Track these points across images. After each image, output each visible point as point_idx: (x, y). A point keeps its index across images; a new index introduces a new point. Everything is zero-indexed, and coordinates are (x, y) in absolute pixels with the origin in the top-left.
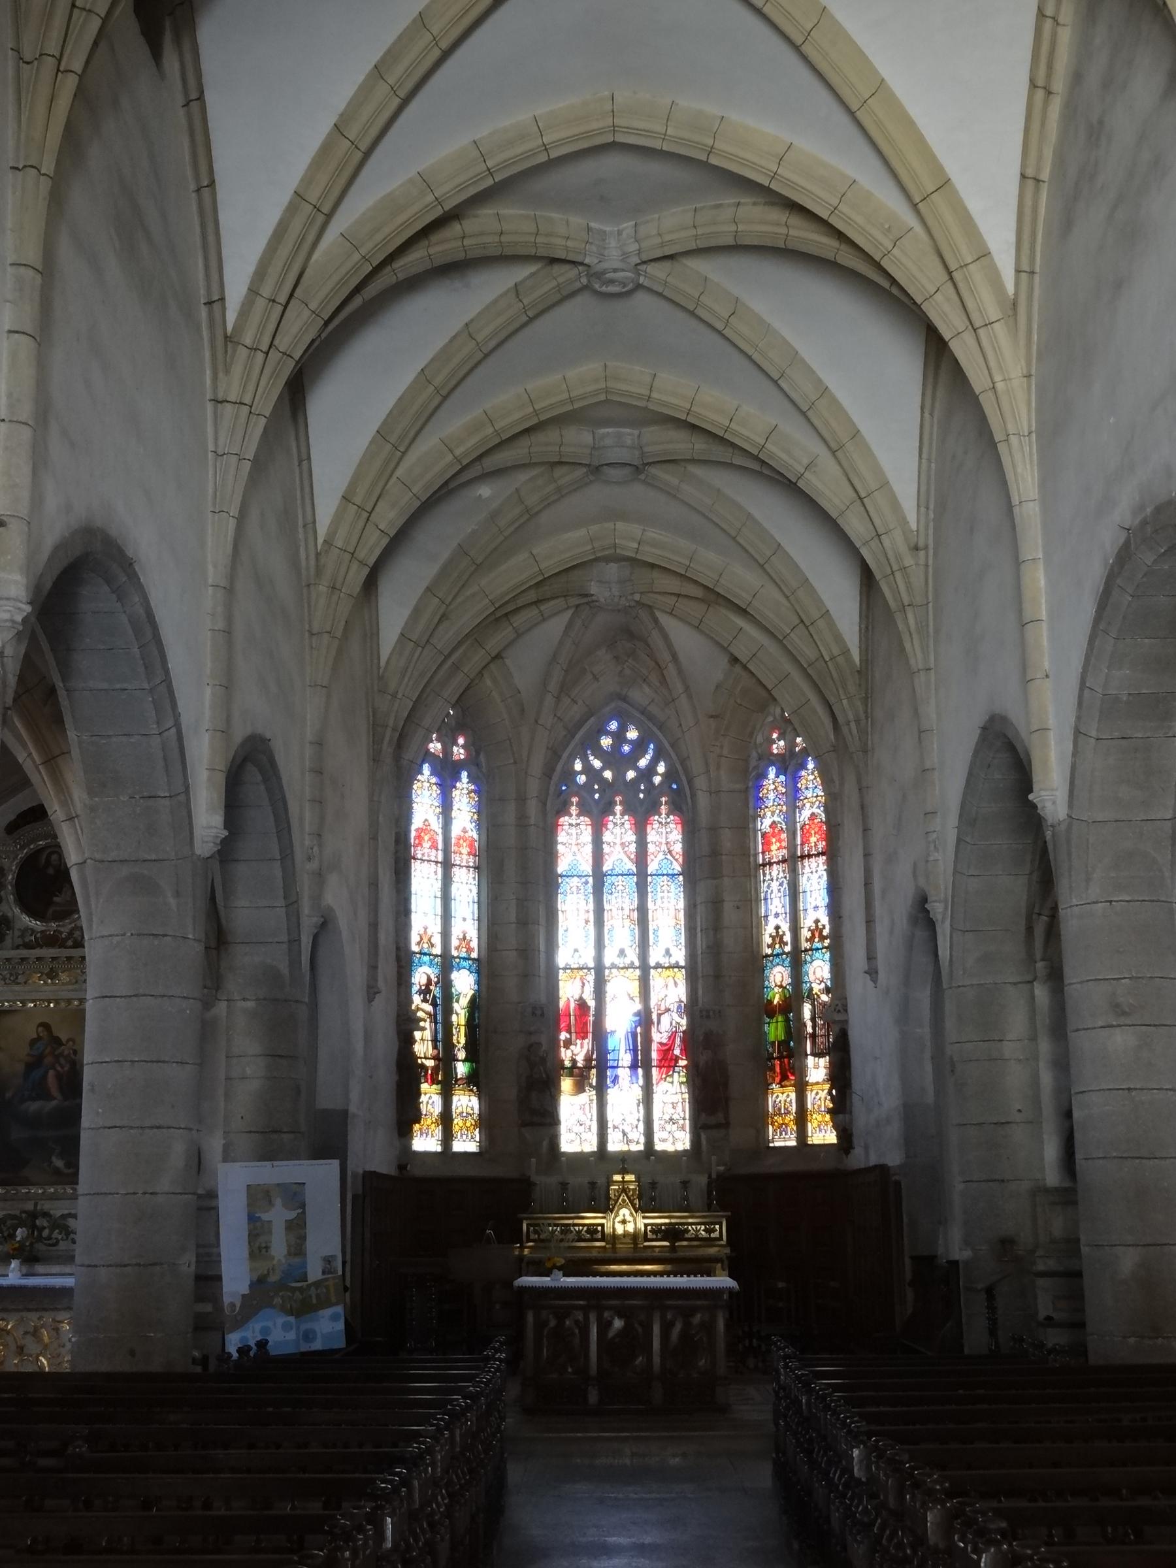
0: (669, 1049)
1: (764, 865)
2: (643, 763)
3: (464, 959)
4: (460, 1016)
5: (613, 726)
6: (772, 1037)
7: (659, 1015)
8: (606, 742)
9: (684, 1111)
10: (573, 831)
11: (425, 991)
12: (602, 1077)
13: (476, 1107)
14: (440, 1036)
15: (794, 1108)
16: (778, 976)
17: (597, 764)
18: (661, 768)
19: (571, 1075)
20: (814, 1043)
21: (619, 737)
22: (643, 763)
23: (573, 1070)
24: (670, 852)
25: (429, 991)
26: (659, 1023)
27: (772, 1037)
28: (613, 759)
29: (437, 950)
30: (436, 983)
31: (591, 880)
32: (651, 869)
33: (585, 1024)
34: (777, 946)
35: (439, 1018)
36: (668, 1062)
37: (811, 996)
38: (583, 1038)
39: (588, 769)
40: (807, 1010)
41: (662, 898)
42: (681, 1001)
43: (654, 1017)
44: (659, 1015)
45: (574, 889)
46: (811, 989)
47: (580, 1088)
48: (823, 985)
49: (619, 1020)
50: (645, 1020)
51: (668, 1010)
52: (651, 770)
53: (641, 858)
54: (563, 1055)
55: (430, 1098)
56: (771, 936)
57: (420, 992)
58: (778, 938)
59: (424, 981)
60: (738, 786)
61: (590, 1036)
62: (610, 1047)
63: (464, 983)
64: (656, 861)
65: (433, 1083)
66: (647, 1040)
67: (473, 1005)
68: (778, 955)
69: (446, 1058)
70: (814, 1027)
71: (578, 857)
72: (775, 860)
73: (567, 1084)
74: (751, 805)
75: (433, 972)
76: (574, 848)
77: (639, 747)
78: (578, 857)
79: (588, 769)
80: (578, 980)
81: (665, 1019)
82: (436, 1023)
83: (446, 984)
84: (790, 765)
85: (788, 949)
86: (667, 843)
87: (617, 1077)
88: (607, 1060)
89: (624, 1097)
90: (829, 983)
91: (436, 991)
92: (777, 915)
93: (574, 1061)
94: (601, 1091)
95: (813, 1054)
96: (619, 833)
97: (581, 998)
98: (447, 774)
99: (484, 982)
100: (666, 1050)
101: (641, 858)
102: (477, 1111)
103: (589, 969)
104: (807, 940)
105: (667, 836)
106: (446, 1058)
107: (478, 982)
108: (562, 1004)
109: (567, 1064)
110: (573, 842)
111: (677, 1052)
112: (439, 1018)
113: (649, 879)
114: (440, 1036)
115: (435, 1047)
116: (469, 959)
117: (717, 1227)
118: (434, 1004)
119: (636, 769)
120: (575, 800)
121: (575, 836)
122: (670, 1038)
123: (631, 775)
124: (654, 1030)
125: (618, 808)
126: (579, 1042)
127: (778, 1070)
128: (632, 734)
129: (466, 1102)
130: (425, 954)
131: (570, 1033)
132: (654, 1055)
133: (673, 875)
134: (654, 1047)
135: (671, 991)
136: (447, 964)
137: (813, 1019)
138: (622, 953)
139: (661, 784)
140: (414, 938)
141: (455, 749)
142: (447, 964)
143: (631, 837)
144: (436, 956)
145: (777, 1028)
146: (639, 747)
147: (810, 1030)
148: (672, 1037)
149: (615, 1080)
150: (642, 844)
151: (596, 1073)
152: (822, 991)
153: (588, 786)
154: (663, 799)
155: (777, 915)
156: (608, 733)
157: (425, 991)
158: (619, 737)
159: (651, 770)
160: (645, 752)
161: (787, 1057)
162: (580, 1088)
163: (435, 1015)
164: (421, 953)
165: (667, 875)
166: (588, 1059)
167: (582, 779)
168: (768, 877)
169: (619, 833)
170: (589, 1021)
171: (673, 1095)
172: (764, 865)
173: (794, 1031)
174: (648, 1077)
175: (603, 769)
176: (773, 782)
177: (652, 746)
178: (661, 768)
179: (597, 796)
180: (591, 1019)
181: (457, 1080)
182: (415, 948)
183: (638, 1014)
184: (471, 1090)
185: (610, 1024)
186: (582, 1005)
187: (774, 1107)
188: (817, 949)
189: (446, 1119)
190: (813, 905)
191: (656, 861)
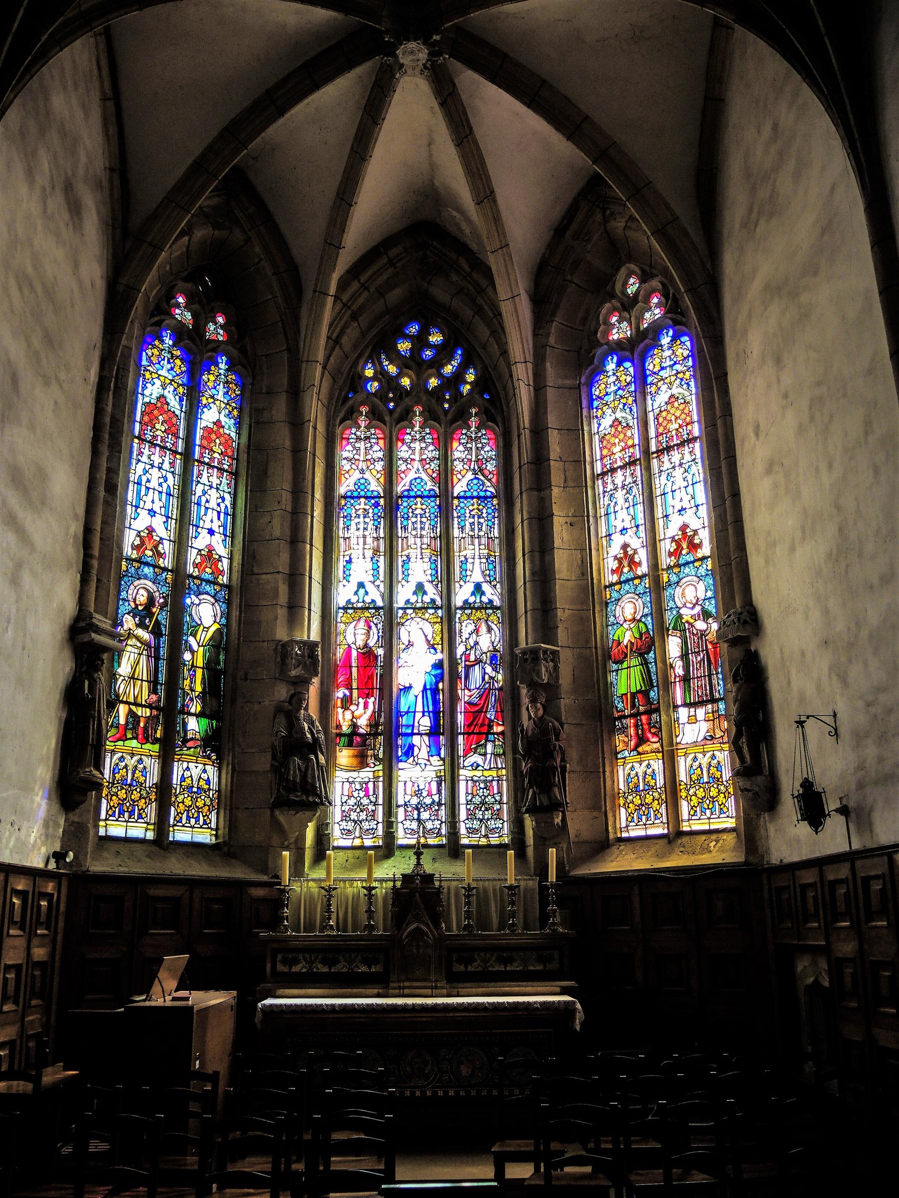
0: (480, 711)
1: (604, 474)
2: (448, 369)
3: (208, 582)
4: (196, 653)
5: (413, 329)
6: (622, 689)
7: (467, 668)
8: (404, 346)
9: (66, 1189)
10: (361, 445)
11: (144, 614)
12: (390, 747)
13: (214, 780)
14: (162, 678)
15: (660, 781)
16: (627, 613)
17: (392, 369)
18: (470, 377)
19: (350, 744)
20: (687, 689)
21: (420, 341)
22: (448, 369)
23: (352, 737)
24: (481, 471)
25: (151, 615)
26: (467, 677)
27: (622, 689)
28: (413, 363)
29: (167, 562)
30: (165, 605)
31: (382, 501)
32: (458, 490)
33: (371, 678)
34: (626, 570)
35: (163, 652)
36: (479, 731)
37: (680, 626)
38: (368, 696)
39: (381, 374)
40: (674, 646)
41: (472, 524)
42: (495, 650)
43: (461, 669)
44: (467, 668)
45: (360, 512)
46: (680, 616)
47: (362, 762)
48: (698, 609)
49: (414, 668)
50: (449, 673)
51: (478, 661)
52: (458, 378)
53: (444, 477)
54: (340, 717)
55: (128, 759)
56: (615, 558)
57: (134, 613)
58: (627, 558)
59: (142, 598)
60: (568, 382)
61: (377, 693)
62: (403, 708)
63: (206, 613)
64: (464, 482)
65: (146, 740)
66: (454, 698)
67: (217, 644)
68: (627, 581)
69: (169, 712)
70: (686, 667)
71: (367, 475)
72: (619, 463)
73: (344, 756)
74: (585, 403)
75: (160, 593)
76: (362, 465)
77: (444, 352)
78: (367, 475)
79: (381, 374)
80: (362, 624)
81: (477, 672)
82: (157, 658)
83: (178, 610)
84: (637, 349)
85: (643, 569)
86: (477, 461)
87: (411, 747)
88: (398, 726)
89: (418, 774)
90: (398, 884)
91: (163, 618)
92: (624, 530)
93: (354, 726)
94: (389, 764)
95: (685, 705)
96: (416, 455)
97: (366, 645)
98: (196, 354)
99: (235, 613)
100: (475, 712)
101: (444, 477)
102: (214, 786)
103: (378, 609)
104: (670, 554)
105: (473, 458)
106: (169, 712)
107: (228, 615)
108: (340, 652)
109: (345, 729)
110: (359, 462)
111: (491, 715)
112: (163, 652)
113: (456, 502)
114: (162, 678)
115: (153, 691)
116: (215, 583)
117: (556, 955)
118: (156, 632)
119: (440, 376)
120: (364, 409)
121: (362, 451)
122: (481, 696)
123: (433, 382)
124: (460, 685)
125: (418, 420)
126: (361, 701)
127: (632, 731)
128: (436, 338)
129: (196, 771)
130: (147, 564)
131: (351, 689)
132: (460, 718)
133: (486, 498)
134: (461, 707)
135: (609, 421)
136: (180, 584)
137: (684, 656)
138: (420, 588)
139: (471, 392)
140: (130, 538)
141: (212, 327)
142: (180, 584)
143: (431, 452)
144: (165, 569)
145: (629, 677)
146: (444, 352)
147: (680, 671)
148: (485, 694)
149: (410, 751)
150: (445, 459)
151: (384, 741)
152: (696, 618)
153: (381, 394)
154: (474, 411)
155: (624, 530)
156: (407, 337)
157: (144, 614)
158: (420, 341)
159: (458, 378)
160: (451, 358)
161: (645, 713)
162: (362, 762)
163: (157, 648)
164: (138, 561)
165: (478, 497)
166: (374, 724)
167: (373, 386)
168: (610, 486)
169: (416, 455)
170: (375, 672)
171: (484, 769)
172: (604, 474)
173: (656, 681)
174: (452, 746)
175: (400, 375)
176: (614, 376)
177: (459, 352)
178: (470, 377)
179: (391, 395)
180: (379, 671)
181: (185, 741)
182: (128, 551)
183: (438, 665)
184: (209, 758)
185: (402, 677)
186: (367, 655)
187: (628, 783)
188: (687, 563)
189: (164, 792)
190: (678, 507)
191: (464, 482)
